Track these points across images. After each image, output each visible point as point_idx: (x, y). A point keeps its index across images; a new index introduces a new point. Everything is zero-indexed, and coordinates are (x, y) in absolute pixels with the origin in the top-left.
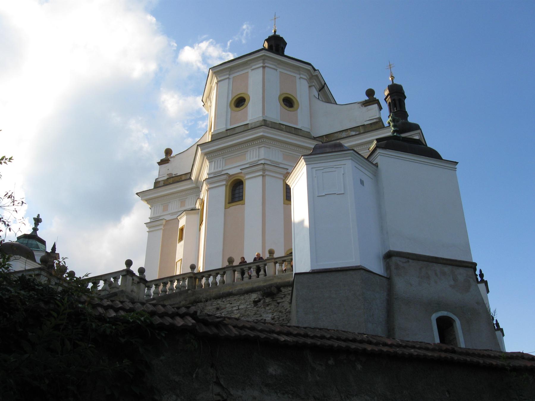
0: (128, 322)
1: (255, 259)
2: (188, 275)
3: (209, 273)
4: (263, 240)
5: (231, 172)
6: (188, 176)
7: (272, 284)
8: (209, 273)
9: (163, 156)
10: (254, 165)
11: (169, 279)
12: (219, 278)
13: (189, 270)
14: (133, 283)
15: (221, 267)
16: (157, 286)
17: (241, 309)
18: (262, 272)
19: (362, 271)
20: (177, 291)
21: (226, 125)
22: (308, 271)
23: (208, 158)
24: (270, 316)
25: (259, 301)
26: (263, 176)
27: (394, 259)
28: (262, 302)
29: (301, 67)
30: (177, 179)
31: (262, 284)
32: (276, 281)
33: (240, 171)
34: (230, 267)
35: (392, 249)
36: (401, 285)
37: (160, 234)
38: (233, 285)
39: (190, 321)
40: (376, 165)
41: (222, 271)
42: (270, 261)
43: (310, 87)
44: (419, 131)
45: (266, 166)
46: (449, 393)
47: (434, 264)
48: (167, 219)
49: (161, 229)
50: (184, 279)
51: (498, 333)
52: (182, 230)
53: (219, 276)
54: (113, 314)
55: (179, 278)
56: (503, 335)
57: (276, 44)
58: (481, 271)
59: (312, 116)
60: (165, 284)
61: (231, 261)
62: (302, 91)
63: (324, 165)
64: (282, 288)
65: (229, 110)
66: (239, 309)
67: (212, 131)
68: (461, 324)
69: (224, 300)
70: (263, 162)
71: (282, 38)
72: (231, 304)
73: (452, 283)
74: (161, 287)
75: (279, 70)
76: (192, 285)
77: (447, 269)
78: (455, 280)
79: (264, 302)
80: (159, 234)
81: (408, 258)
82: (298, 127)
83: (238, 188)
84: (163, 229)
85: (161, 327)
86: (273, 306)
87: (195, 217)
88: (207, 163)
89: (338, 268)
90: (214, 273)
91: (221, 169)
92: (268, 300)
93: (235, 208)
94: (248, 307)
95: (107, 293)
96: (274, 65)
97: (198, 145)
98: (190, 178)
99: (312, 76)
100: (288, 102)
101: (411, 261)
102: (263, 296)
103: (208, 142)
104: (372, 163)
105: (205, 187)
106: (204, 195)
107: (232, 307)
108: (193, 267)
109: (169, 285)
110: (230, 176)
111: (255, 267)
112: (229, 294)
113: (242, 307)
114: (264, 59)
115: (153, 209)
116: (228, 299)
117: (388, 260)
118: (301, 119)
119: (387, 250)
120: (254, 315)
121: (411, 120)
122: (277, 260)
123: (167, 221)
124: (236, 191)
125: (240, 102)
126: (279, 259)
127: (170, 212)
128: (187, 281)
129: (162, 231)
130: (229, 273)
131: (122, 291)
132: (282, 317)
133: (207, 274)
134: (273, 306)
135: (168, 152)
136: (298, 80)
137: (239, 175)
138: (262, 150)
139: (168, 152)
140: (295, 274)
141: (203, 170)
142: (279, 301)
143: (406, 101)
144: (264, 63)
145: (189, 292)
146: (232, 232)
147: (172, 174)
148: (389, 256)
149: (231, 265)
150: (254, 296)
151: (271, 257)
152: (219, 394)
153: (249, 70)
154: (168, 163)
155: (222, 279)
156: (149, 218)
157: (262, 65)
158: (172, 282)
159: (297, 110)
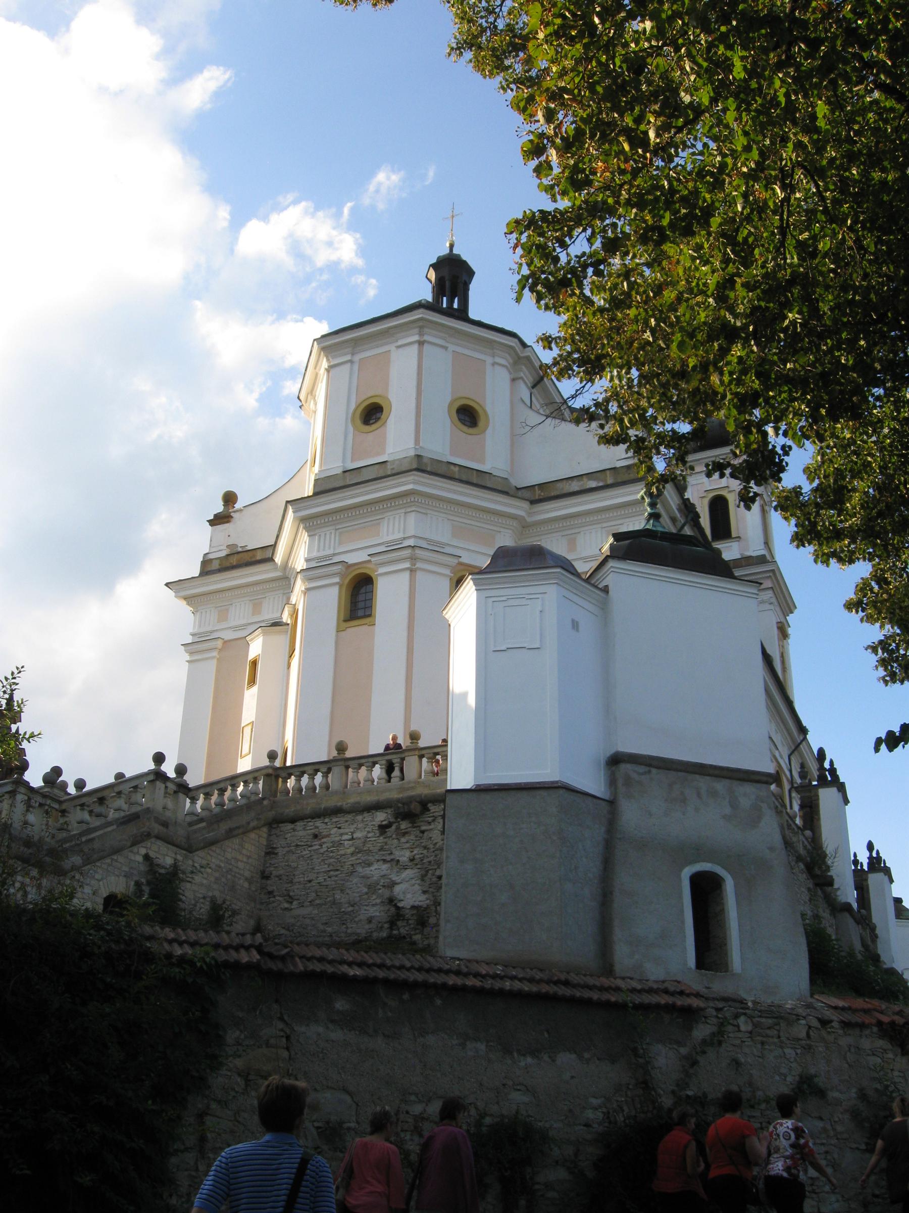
0: (192, 963)
1: (387, 748)
2: (265, 772)
3: (302, 769)
4: (406, 699)
5: (351, 559)
7: (412, 797)
8: (302, 769)
9: (219, 508)
10: (394, 548)
11: (228, 782)
12: (319, 778)
13: (266, 762)
14: (166, 793)
15: (325, 759)
16: (208, 795)
17: (357, 838)
18: (396, 773)
19: (561, 791)
20: (244, 801)
21: (344, 461)
22: (468, 787)
23: (307, 529)
24: (407, 854)
25: (389, 826)
26: (412, 571)
27: (624, 767)
28: (394, 827)
29: (495, 341)
30: (247, 557)
31: (395, 795)
32: (421, 791)
33: (369, 558)
34: (342, 760)
36: (631, 815)
37: (212, 666)
38: (344, 793)
39: (255, 956)
40: (606, 590)
41: (326, 767)
42: (411, 753)
43: (513, 380)
45: (418, 551)
46: (548, 1032)
47: (697, 776)
48: (226, 639)
49: (213, 657)
50: (256, 780)
52: (254, 663)
53: (320, 774)
54: (178, 951)
55: (250, 776)
56: (891, 881)
58: (831, 763)
59: (515, 438)
60: (222, 791)
61: (341, 748)
64: (429, 805)
65: (351, 429)
66: (353, 839)
68: (736, 886)
69: (326, 820)
70: (411, 542)
71: (465, 263)
72: (340, 828)
73: (728, 811)
74: (215, 798)
75: (452, 348)
76: (271, 791)
77: (720, 786)
78: (734, 805)
79: (398, 828)
80: (210, 667)
81: (650, 765)
83: (363, 590)
84: (219, 660)
85: (226, 964)
86: (412, 837)
87: (280, 640)
88: (304, 537)
89: (520, 784)
90: (310, 770)
91: (331, 552)
92: (404, 825)
93: (357, 631)
94: (370, 835)
95: (122, 814)
96: (441, 338)
97: (288, 502)
98: (271, 560)
99: (519, 358)
100: (468, 415)
101: (654, 771)
102: (396, 818)
103: (309, 497)
104: (596, 587)
105: (299, 585)
106: (298, 596)
107: (341, 835)
108: (272, 756)
109: (228, 794)
110: (349, 566)
111: (384, 762)
112: (337, 811)
114: (421, 325)
115: (198, 614)
116: (335, 820)
117: (614, 768)
118: (492, 453)
119: (613, 751)
120: (380, 850)
122: (424, 752)
123: (226, 642)
124: (359, 597)
125: (372, 413)
126: (428, 751)
127: (232, 624)
128: (261, 782)
129: (215, 662)
130: (337, 770)
131: (148, 810)
132: (428, 857)
133: (299, 770)
134: (412, 837)
135: (229, 498)
136: (489, 367)
137: (365, 565)
138: (412, 518)
139: (229, 498)
141: (297, 549)
142: (423, 828)
144: (421, 334)
145: (265, 802)
146: (347, 687)
147: (236, 546)
148: (615, 761)
149: (342, 756)
150: (381, 817)
151: (413, 746)
152: (282, 1030)
153: (392, 347)
154: (228, 522)
155: (324, 781)
156: (193, 635)
157: (416, 338)
158: (234, 787)
159: (484, 431)
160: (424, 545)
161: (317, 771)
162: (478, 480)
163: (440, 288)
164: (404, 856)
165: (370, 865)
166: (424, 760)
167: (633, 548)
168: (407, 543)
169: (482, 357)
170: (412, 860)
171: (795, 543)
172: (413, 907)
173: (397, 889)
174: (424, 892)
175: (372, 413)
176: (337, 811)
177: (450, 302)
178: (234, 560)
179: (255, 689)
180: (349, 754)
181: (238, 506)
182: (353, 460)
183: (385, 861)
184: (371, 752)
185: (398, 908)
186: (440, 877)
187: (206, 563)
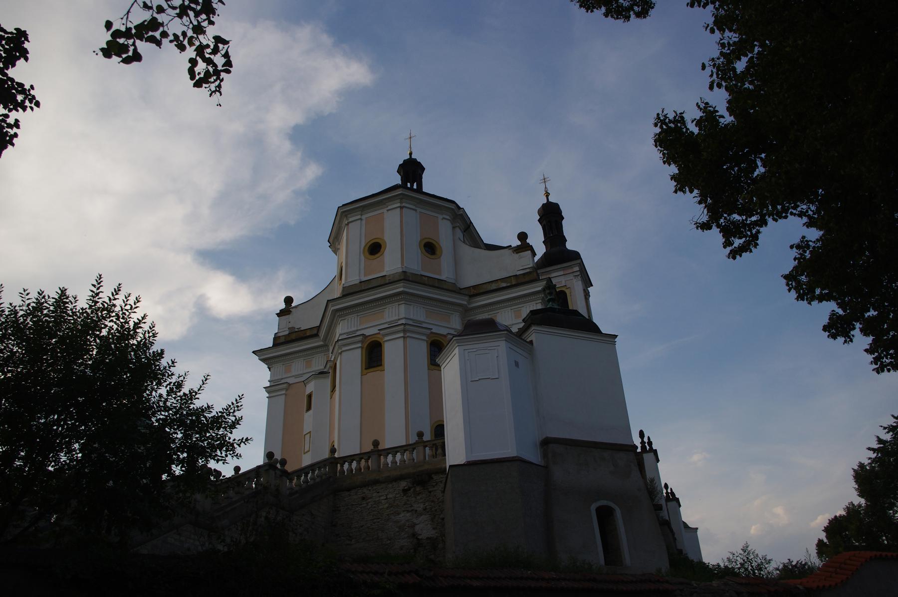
5: (368, 332)
6: (315, 332)
9: (283, 306)
10: (392, 327)
24: (422, 506)
34: (377, 451)
35: (549, 436)
40: (531, 342)
43: (454, 228)
44: (579, 261)
45: (407, 327)
51: (672, 504)
53: (363, 461)
56: (680, 506)
57: (411, 170)
58: (649, 438)
61: (376, 443)
62: (445, 234)
63: (477, 346)
67: (343, 281)
70: (403, 321)
75: (419, 210)
82: (443, 277)
93: (373, 375)
100: (430, 248)
112: (376, 482)
113: (390, 496)
114: (402, 197)
121: (570, 246)
125: (375, 249)
133: (350, 458)
140: (450, 466)
143: (564, 222)
146: (371, 408)
148: (546, 442)
150: (403, 484)
153: (385, 210)
157: (399, 205)
160: (411, 323)
161: (362, 458)
162: (438, 284)
163: (405, 180)
164: (419, 507)
165: (399, 514)
166: (427, 449)
167: (535, 319)
168: (400, 322)
169: (436, 215)
170: (425, 509)
171: (154, 348)
172: (428, 538)
173: (417, 528)
174: (434, 529)
175: (375, 249)
176: (376, 482)
177: (412, 185)
178: (293, 336)
179: (311, 412)
180: (380, 447)
181: (293, 305)
182: (365, 276)
183: (408, 511)
184: (387, 447)
185: (418, 539)
186: (443, 519)
187: (276, 338)
